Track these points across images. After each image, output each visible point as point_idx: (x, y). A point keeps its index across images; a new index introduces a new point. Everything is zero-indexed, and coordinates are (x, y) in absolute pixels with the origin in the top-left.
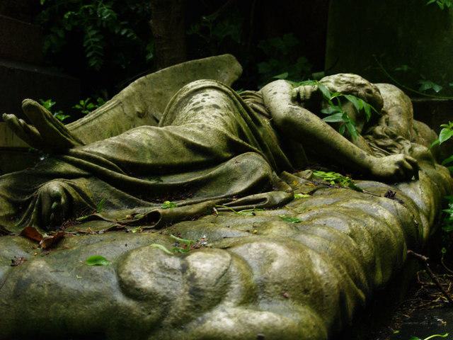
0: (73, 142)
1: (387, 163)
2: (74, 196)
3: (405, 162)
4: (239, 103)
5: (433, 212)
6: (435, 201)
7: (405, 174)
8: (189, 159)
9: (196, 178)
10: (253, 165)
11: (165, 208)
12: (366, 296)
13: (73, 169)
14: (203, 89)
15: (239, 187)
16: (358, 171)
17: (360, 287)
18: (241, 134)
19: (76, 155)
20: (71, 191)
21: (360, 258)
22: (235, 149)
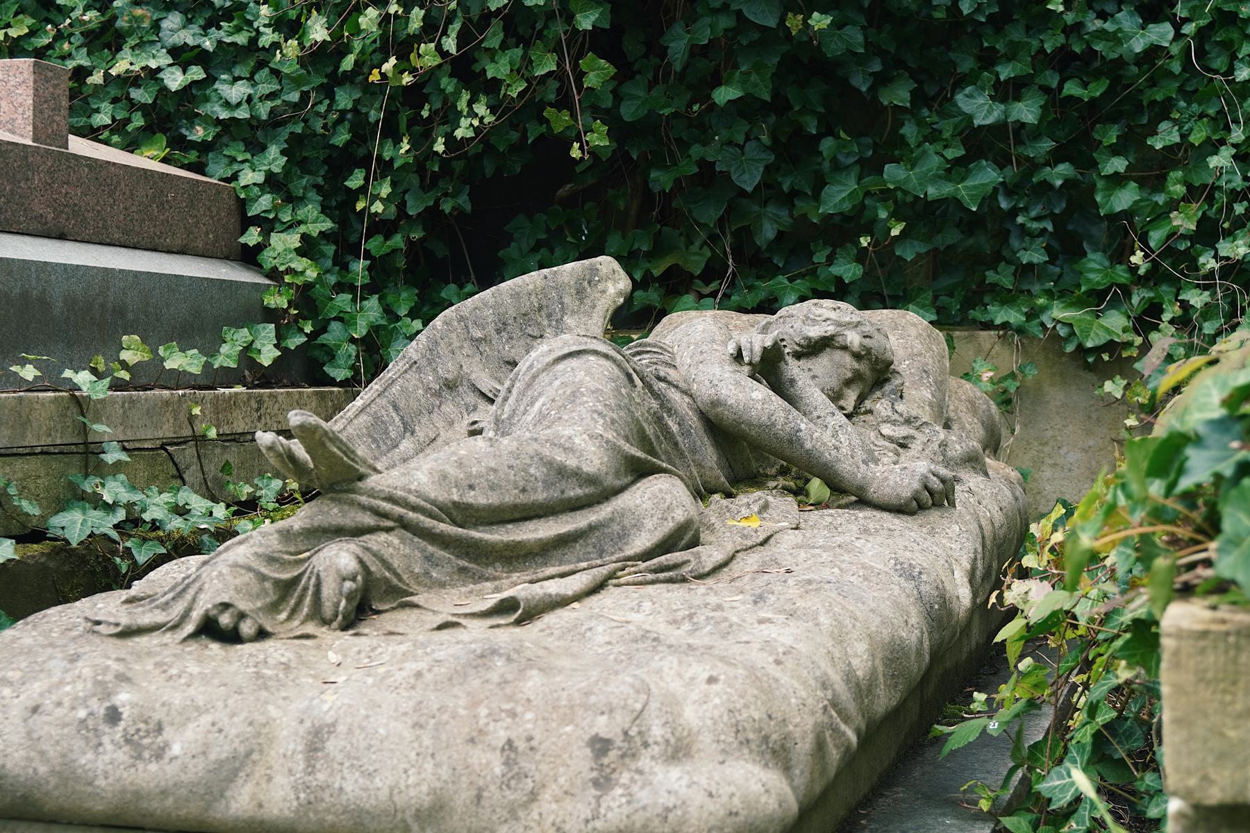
0: (362, 470)
1: (898, 475)
2: (373, 569)
3: (931, 476)
4: (411, 515)
5: (980, 565)
6: (842, 759)
7: (932, 499)
8: (545, 495)
9: (575, 526)
10: (659, 501)
11: (520, 588)
12: (858, 738)
13: (368, 520)
14: (595, 353)
15: (641, 542)
16: (848, 494)
17: (846, 719)
18: (644, 441)
19: (372, 494)
20: (367, 558)
21: (849, 677)
22: (639, 471)
